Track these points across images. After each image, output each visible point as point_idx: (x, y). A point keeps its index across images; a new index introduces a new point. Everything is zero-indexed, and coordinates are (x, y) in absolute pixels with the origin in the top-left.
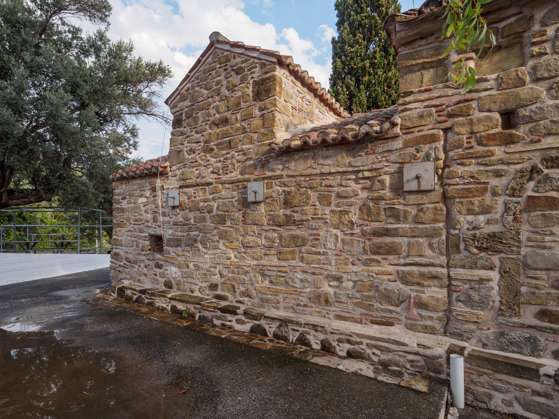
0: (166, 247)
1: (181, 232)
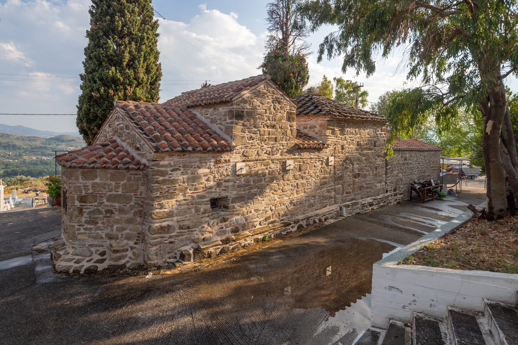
0: (231, 204)
1: (243, 191)
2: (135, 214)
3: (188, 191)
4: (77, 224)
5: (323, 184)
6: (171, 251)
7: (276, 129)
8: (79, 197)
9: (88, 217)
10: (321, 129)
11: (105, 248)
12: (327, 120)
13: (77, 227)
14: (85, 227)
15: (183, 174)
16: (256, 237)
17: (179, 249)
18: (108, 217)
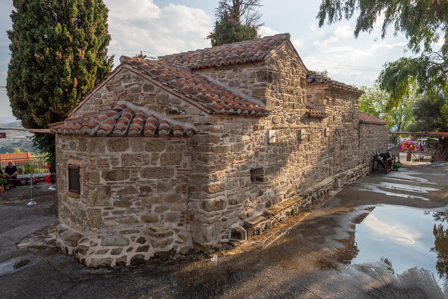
2: (178, 190)
3: (235, 161)
4: (104, 207)
5: (322, 155)
6: (224, 230)
7: (293, 95)
8: (105, 174)
9: (118, 198)
10: (318, 99)
11: (142, 233)
12: (326, 89)
13: (103, 211)
14: (114, 210)
15: (231, 141)
16: (286, 210)
17: (230, 227)
18: (144, 196)
